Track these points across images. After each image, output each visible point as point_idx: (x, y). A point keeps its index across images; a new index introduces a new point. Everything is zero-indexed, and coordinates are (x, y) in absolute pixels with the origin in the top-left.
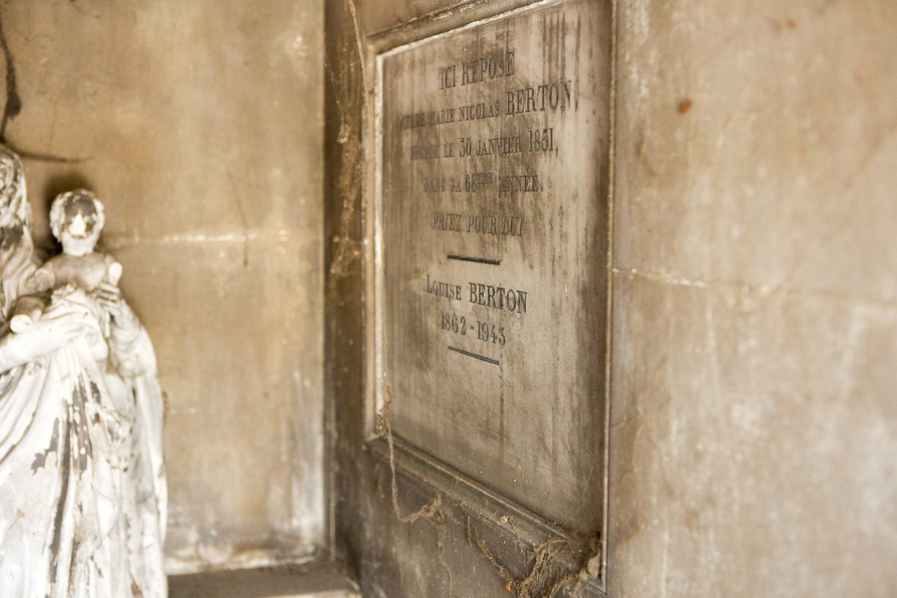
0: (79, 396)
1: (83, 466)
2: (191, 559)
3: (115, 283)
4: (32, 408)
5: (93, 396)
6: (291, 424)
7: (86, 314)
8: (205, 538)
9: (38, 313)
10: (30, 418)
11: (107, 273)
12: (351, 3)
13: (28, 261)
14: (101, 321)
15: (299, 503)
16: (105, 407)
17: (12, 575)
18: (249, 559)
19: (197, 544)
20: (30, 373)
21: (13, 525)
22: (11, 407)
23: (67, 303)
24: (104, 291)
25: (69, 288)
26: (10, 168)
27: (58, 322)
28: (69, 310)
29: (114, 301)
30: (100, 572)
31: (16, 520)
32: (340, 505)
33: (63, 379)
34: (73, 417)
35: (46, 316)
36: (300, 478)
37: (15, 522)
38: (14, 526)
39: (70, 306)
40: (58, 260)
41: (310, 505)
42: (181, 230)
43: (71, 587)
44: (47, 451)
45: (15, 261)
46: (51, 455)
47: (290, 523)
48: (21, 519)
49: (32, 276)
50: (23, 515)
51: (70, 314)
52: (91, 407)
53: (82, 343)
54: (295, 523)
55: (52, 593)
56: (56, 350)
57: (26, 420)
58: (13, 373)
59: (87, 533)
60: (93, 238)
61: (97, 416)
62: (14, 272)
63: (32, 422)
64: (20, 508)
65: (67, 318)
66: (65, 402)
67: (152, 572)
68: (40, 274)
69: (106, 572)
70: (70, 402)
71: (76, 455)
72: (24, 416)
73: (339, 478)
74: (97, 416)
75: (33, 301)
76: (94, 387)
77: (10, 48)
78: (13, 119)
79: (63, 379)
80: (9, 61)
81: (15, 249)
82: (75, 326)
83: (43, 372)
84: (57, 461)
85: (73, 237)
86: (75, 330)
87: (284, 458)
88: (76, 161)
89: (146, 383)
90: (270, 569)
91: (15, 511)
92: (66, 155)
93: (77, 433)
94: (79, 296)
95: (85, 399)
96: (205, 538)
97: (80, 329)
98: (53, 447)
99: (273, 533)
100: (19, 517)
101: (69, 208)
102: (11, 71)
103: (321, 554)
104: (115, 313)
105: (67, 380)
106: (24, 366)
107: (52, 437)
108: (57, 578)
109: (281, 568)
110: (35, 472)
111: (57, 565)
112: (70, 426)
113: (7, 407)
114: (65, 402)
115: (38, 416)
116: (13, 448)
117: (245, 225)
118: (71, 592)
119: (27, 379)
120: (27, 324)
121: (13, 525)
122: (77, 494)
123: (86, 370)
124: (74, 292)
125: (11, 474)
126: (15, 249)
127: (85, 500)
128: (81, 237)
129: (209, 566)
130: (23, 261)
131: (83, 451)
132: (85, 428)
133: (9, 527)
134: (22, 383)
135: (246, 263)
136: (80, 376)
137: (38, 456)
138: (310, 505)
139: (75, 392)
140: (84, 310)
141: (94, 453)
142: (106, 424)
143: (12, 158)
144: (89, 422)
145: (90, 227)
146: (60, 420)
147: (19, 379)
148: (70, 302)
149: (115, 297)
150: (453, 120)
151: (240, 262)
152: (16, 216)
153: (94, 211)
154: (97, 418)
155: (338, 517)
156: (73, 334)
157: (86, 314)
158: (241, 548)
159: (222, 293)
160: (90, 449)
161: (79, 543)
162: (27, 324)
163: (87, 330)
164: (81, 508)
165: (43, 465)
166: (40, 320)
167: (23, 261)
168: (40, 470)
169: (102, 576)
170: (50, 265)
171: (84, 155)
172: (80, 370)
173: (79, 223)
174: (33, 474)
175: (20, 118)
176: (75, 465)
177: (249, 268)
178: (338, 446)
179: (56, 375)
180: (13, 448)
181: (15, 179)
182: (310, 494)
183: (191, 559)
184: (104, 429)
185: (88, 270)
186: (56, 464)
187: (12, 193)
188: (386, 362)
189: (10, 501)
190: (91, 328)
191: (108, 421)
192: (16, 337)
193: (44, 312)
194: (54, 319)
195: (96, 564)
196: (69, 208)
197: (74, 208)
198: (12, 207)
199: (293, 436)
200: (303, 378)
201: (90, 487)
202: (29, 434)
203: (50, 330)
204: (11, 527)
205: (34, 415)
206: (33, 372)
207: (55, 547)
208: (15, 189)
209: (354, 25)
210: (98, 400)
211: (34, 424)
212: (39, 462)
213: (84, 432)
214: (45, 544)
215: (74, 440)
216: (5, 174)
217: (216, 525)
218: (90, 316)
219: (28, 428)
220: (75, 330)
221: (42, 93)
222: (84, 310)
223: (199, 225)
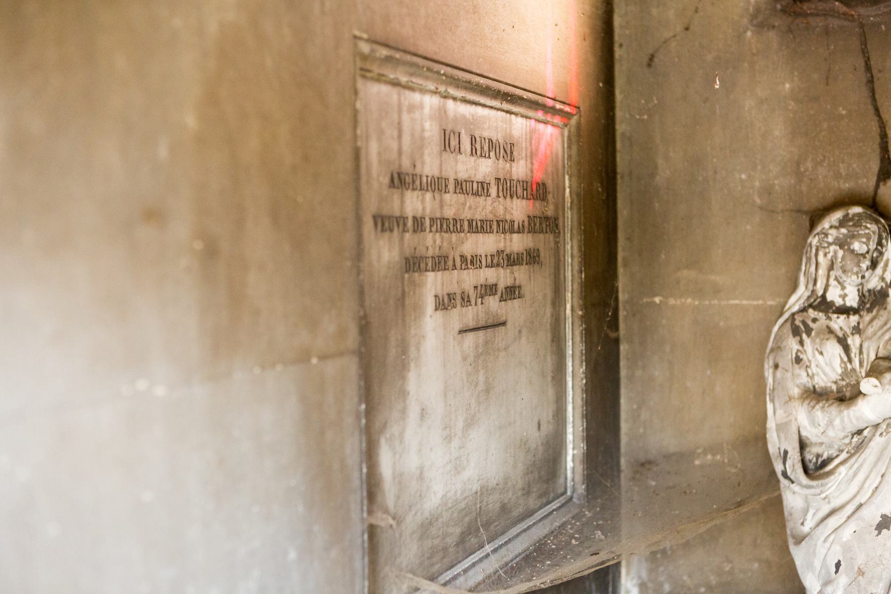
10: (879, 479)
20: (881, 434)
21: (852, 582)
22: (861, 465)
26: (874, 233)
31: (856, 578)
38: (854, 583)
50: (863, 573)
57: (874, 481)
58: (866, 433)
62: (875, 334)
63: (880, 483)
64: (861, 567)
72: (872, 476)
77: (883, 116)
78: (885, 184)
81: (878, 311)
91: (856, 569)
106: (877, 426)
110: (879, 533)
113: (856, 466)
115: (886, 478)
120: (876, 386)
121: (852, 582)
125: (855, 532)
126: (878, 311)
133: (849, 584)
143: (877, 222)
150: (520, 296)
152: (883, 279)
162: (876, 386)
168: (885, 531)
174: (877, 535)
188: (564, 441)
192: (868, 398)
204: (850, 585)
205: (882, 476)
206: (884, 434)
209: (584, 214)
216: (869, 239)
219: (876, 488)
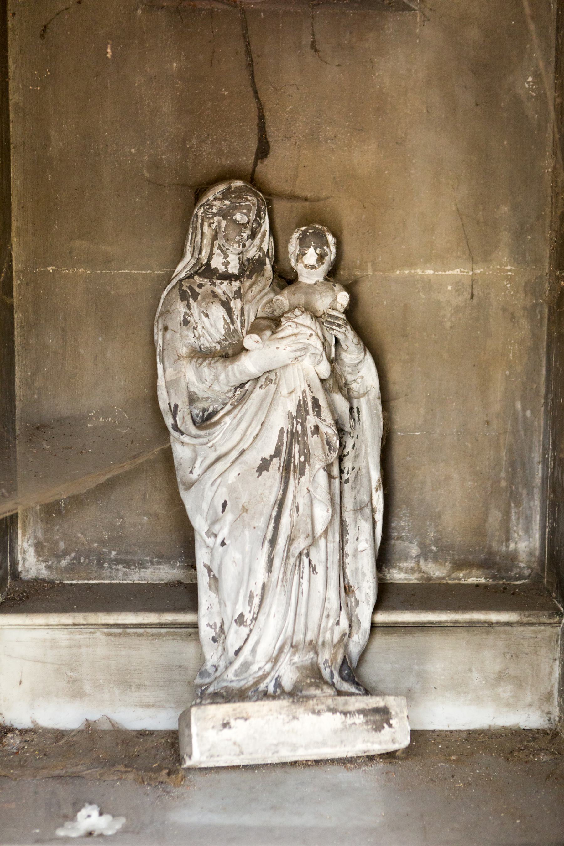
0: (302, 408)
1: (302, 473)
2: (412, 570)
3: (342, 310)
4: (261, 417)
5: (313, 411)
6: (511, 451)
7: (311, 335)
8: (425, 554)
9: (268, 333)
11: (335, 300)
12: (526, 3)
13: (267, 289)
14: (325, 343)
15: (517, 530)
16: (325, 421)
17: (234, 562)
18: (466, 576)
19: (418, 556)
22: (244, 415)
23: (294, 325)
24: (330, 316)
25: (297, 312)
27: (285, 342)
28: (296, 331)
29: (339, 326)
30: (314, 569)
32: (553, 532)
33: (290, 393)
34: (296, 427)
35: (275, 336)
36: (518, 504)
37: (239, 517)
39: (297, 327)
40: (292, 288)
41: (527, 530)
42: (411, 265)
43: (285, 578)
44: (272, 457)
45: (256, 288)
46: (275, 460)
47: (507, 547)
48: (244, 514)
49: (271, 301)
50: (247, 510)
51: (295, 335)
52: (312, 420)
53: (307, 363)
54: (512, 546)
55: (268, 581)
56: (286, 366)
57: (255, 429)
59: (301, 531)
60: (323, 269)
61: (317, 428)
63: (260, 430)
64: (245, 505)
65: (293, 337)
66: (290, 414)
67: (364, 574)
68: (277, 300)
69: (320, 569)
70: (295, 414)
71: (297, 462)
72: (253, 424)
73: (553, 505)
74: (317, 428)
75: (265, 323)
76: (315, 401)
79: (290, 393)
80: (261, 109)
82: (301, 346)
83: (273, 387)
84: (280, 466)
85: (306, 266)
86: (300, 350)
87: (503, 484)
88: (318, 200)
89: (368, 402)
90: (486, 587)
92: (309, 194)
93: (298, 442)
94: (306, 319)
95: (307, 413)
96: (425, 554)
97: (305, 349)
98: (277, 453)
99: (491, 553)
100: (243, 512)
101: (303, 242)
102: (262, 117)
103: (537, 579)
104: (340, 336)
105: (293, 394)
107: (277, 444)
108: (272, 569)
109: (495, 587)
110: (260, 475)
111: (273, 557)
112: (293, 435)
113: (239, 416)
114: (290, 414)
115: (265, 425)
116: (243, 451)
117: (473, 260)
118: (284, 582)
119: (258, 393)
120: (257, 342)
122: (294, 497)
123: (309, 386)
124: (301, 315)
125: (239, 474)
126: (257, 278)
127: (302, 501)
128: (313, 267)
129: (429, 579)
130: (263, 289)
131: (302, 459)
132: (306, 438)
134: (253, 396)
135: (472, 296)
136: (304, 392)
137: (264, 460)
138: (527, 530)
139: (299, 406)
140: (309, 332)
141: (312, 461)
142: (325, 436)
143: (256, 195)
144: (309, 432)
145: (321, 258)
146: (285, 430)
147: (252, 392)
148: (297, 324)
149: (340, 322)
151: (467, 295)
152: (260, 249)
153: (327, 244)
154: (317, 429)
155: (551, 542)
156: (298, 353)
157: (311, 335)
158: (458, 566)
159: (448, 325)
160: (307, 457)
161: (293, 540)
163: (312, 350)
164: (297, 509)
165: (268, 470)
166: (270, 339)
167: (263, 289)
168: (265, 473)
169: (317, 573)
170: (285, 292)
171: (324, 194)
172: (304, 386)
173: (311, 256)
174: (258, 477)
175: (268, 161)
176: (295, 471)
177: (476, 300)
178: (553, 473)
179: (284, 391)
180: (243, 451)
181: (258, 215)
182: (529, 520)
183: (412, 570)
184: (322, 441)
185: (318, 297)
186: (279, 469)
187: (257, 228)
189: (236, 498)
190: (315, 348)
191: (326, 433)
192: (250, 354)
193: (273, 333)
194: (282, 338)
195: (310, 562)
196: (303, 242)
197: (308, 240)
198: (257, 241)
199: (512, 464)
200: (524, 410)
201: (306, 491)
202: (257, 440)
203: (277, 348)
205: (262, 424)
206: (264, 386)
207: (273, 542)
208: (260, 225)
210: (318, 414)
211: (262, 431)
212: (264, 466)
213: (305, 441)
214: (264, 538)
215: (296, 449)
216: (249, 210)
217: (437, 542)
218: (314, 338)
219: (257, 435)
220: (300, 350)
221: (288, 138)
222: (309, 332)
223: (428, 260)
